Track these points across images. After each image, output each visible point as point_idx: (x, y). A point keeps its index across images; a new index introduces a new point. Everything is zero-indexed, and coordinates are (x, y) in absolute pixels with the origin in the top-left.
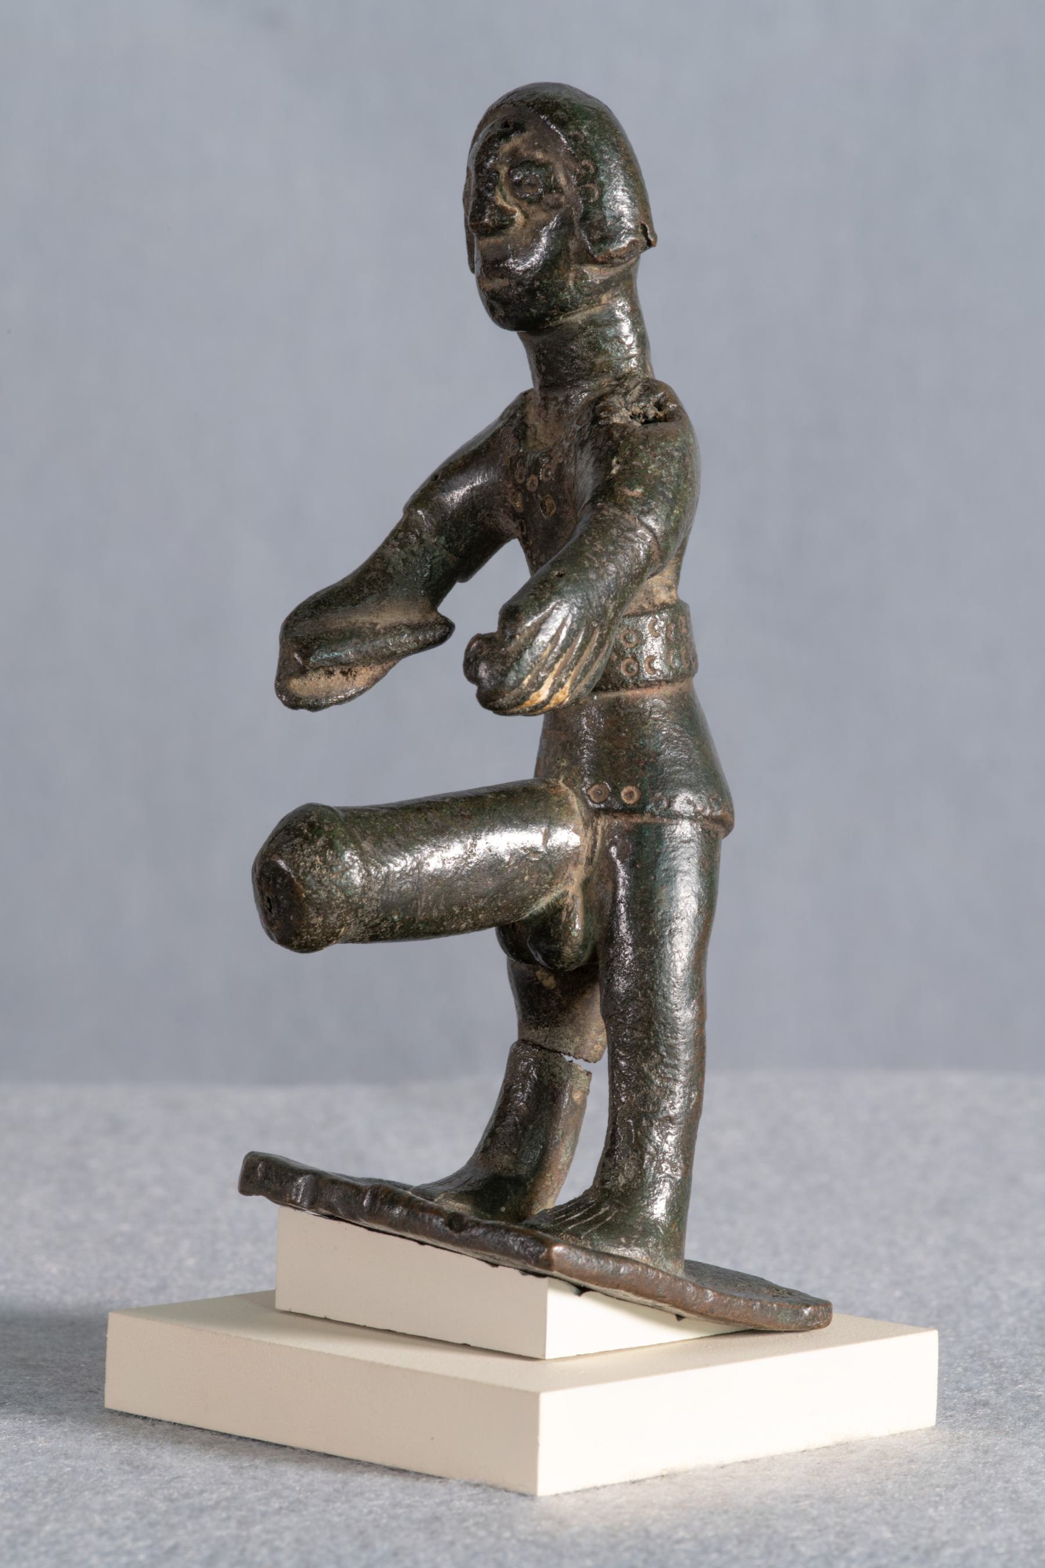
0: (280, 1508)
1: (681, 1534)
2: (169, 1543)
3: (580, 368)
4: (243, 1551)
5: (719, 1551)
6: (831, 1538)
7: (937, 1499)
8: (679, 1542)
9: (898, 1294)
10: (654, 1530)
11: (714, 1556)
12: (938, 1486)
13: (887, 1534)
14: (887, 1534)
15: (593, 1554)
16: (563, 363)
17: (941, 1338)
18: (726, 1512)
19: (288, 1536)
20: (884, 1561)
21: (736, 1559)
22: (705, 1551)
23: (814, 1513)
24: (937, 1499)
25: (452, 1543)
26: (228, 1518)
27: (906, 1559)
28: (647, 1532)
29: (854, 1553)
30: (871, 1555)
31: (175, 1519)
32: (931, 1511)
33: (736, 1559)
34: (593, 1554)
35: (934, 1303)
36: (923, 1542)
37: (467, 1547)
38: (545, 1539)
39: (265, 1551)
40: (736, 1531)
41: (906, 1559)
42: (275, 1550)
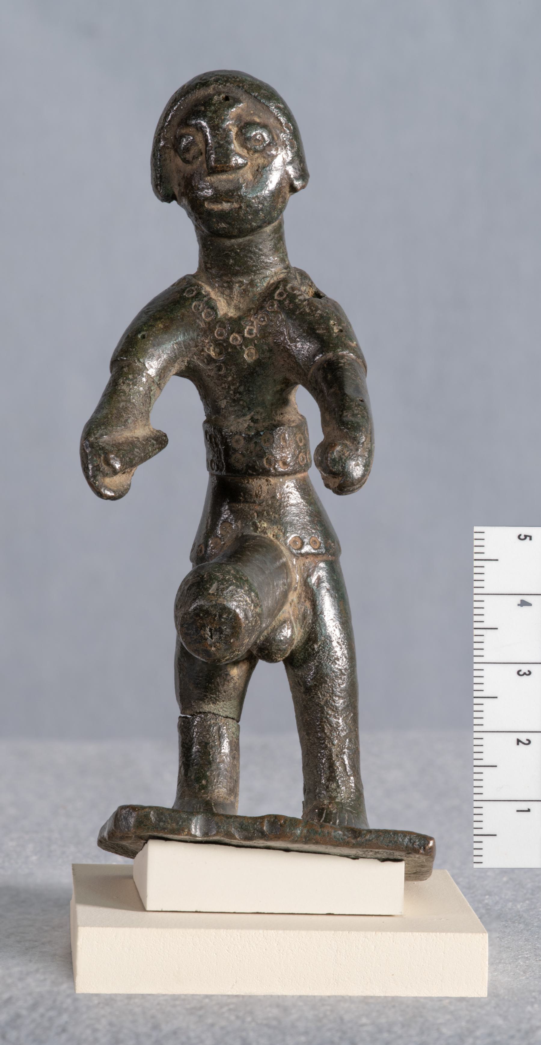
0: (99, 1003)
1: (364, 1020)
2: (6, 996)
3: (263, 262)
4: (55, 1001)
5: (389, 1031)
6: (463, 1024)
7: (533, 1000)
8: (363, 1025)
9: (505, 879)
10: (347, 1017)
11: (386, 1035)
12: (534, 991)
13: (500, 1022)
14: (500, 1022)
15: (306, 1033)
16: (251, 258)
17: (304, 385)
18: (394, 1006)
19: (104, 1022)
20: (498, 1038)
21: (400, 1037)
22: (380, 1031)
23: (452, 1008)
24: (533, 1000)
25: (212, 1025)
26: (45, 980)
27: (512, 1037)
28: (342, 1019)
29: (478, 1033)
30: (490, 1035)
31: (9, 981)
32: (529, 1008)
33: (400, 1037)
34: (306, 1033)
35: (529, 886)
36: (524, 1026)
37: (222, 1028)
38: (274, 1023)
39: (89, 1032)
40: (401, 1019)
41: (512, 1037)
42: (95, 1030)
